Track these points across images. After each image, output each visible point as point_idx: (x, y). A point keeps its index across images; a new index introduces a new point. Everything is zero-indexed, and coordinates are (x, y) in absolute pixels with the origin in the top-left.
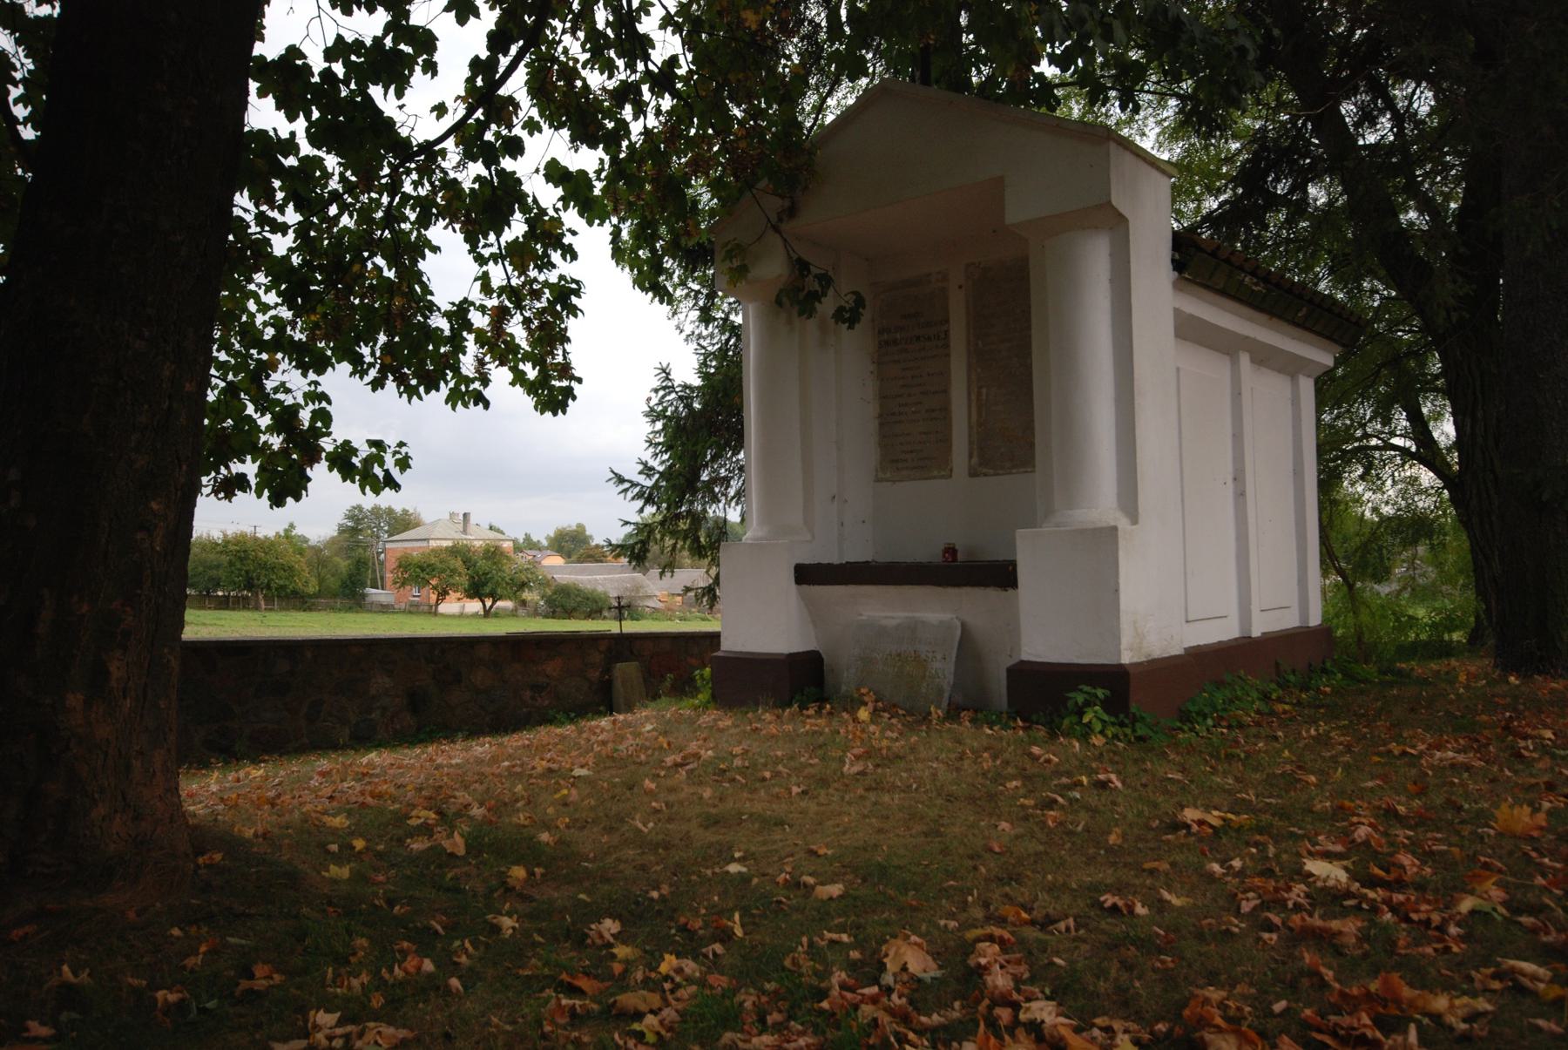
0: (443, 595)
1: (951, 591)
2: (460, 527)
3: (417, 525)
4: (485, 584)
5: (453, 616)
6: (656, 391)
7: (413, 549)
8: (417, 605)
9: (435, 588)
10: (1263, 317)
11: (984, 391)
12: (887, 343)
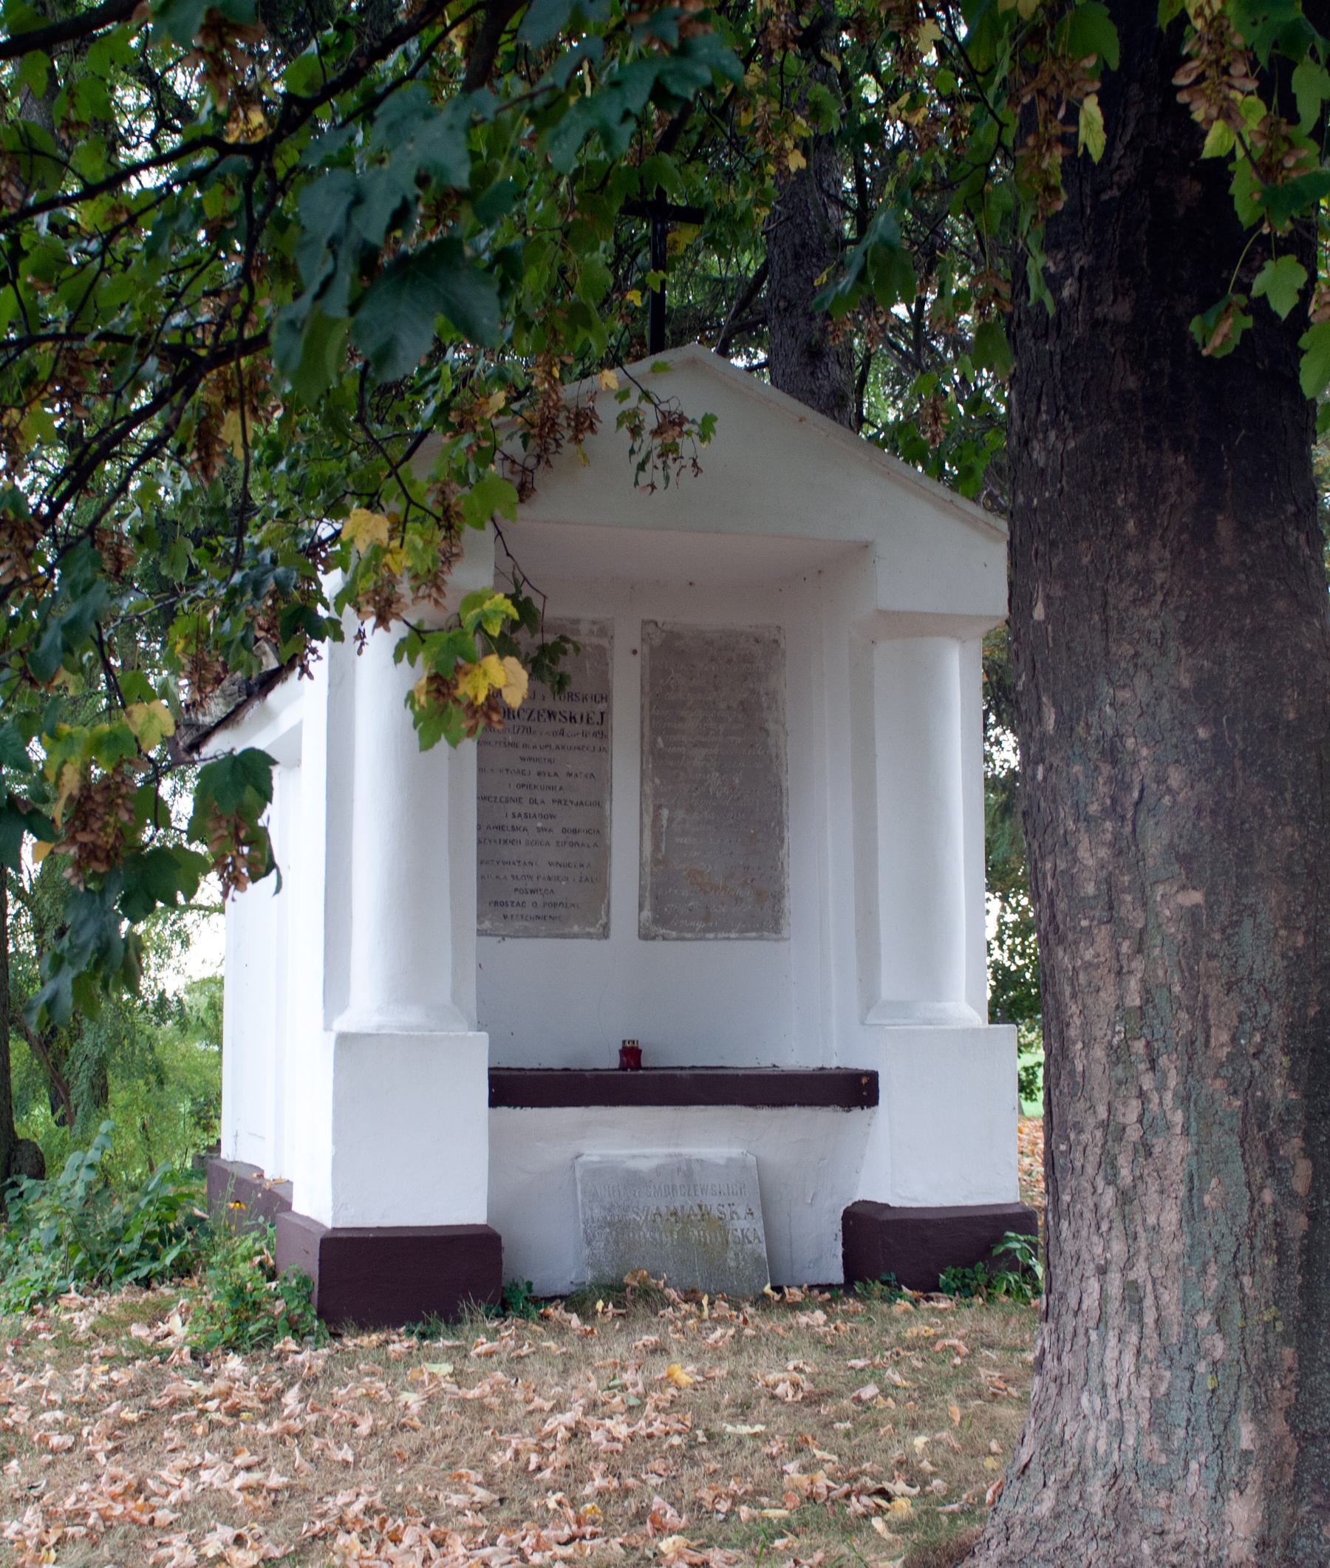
1: (765, 1113)
11: (665, 813)
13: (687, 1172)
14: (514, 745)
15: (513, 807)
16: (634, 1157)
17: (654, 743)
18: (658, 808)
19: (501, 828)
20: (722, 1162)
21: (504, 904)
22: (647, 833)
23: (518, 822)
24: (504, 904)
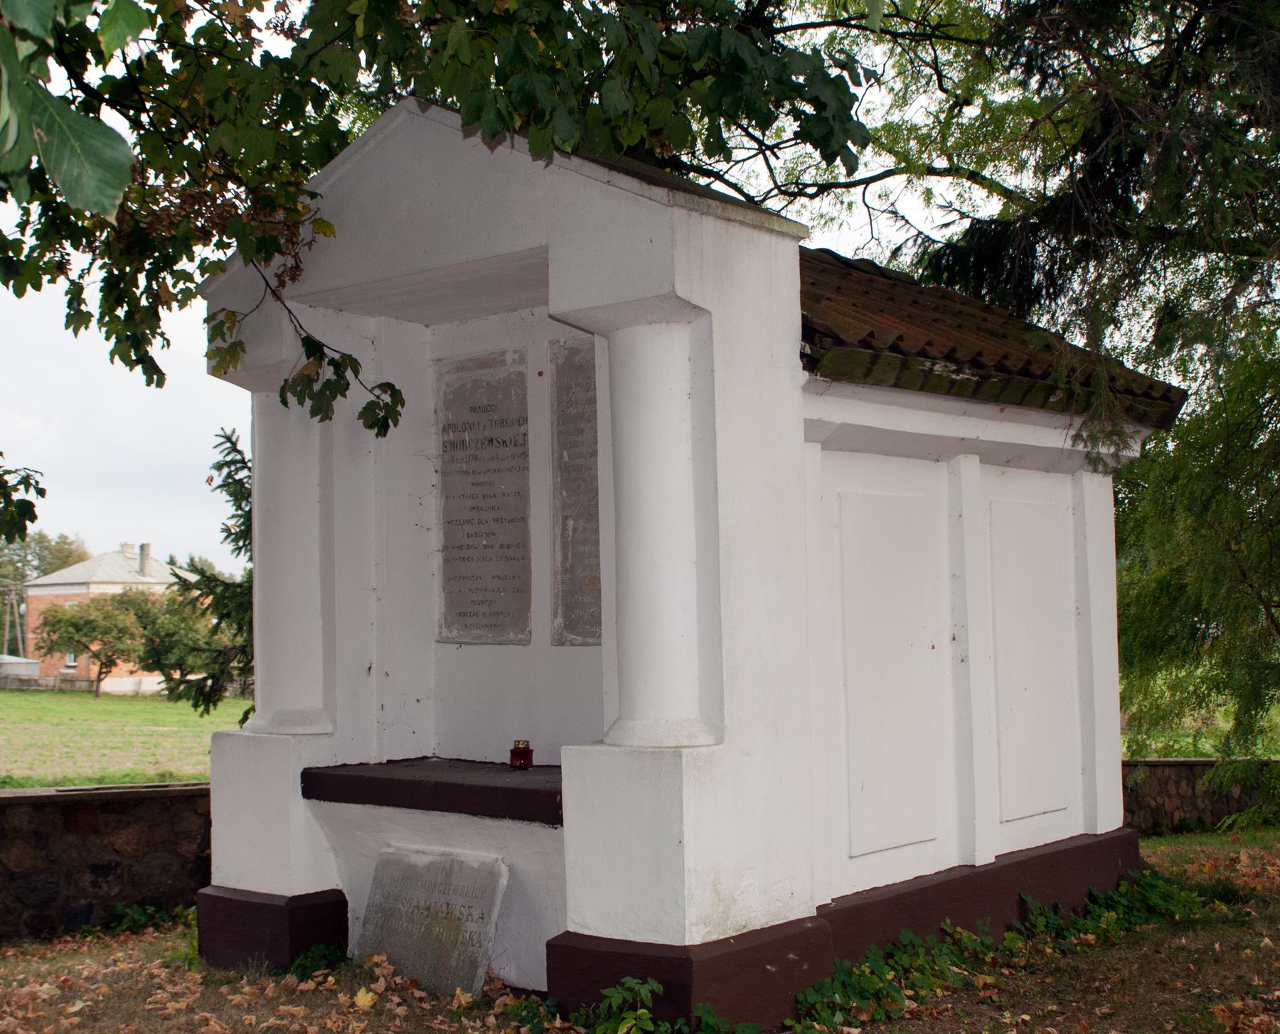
0: (108, 665)
1: (488, 822)
2: (136, 565)
3: (81, 557)
4: (169, 650)
5: (122, 698)
6: (219, 467)
7: (67, 597)
8: (71, 681)
9: (96, 655)
10: (991, 409)
11: (571, 523)
12: (454, 445)
13: (448, 871)
14: (466, 473)
15: (468, 529)
16: (418, 852)
17: (561, 457)
18: (566, 518)
19: (461, 547)
20: (476, 865)
21: (465, 614)
22: (558, 543)
23: (470, 541)
24: (465, 614)
